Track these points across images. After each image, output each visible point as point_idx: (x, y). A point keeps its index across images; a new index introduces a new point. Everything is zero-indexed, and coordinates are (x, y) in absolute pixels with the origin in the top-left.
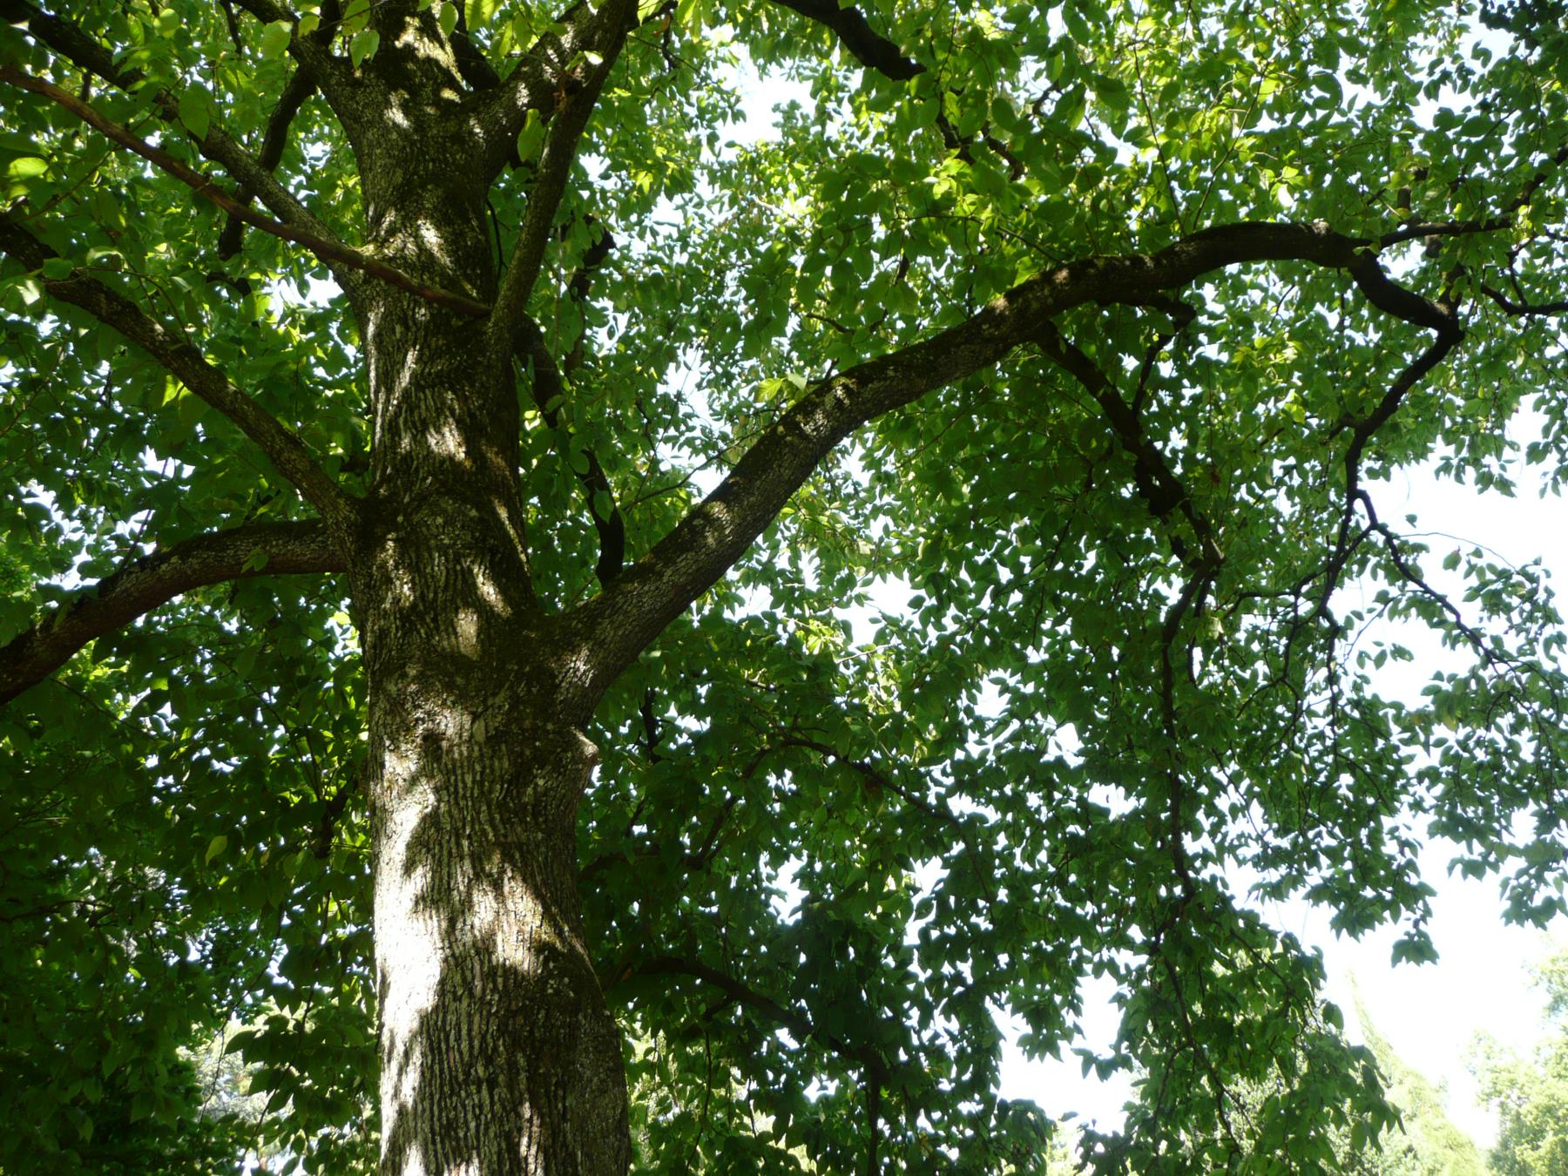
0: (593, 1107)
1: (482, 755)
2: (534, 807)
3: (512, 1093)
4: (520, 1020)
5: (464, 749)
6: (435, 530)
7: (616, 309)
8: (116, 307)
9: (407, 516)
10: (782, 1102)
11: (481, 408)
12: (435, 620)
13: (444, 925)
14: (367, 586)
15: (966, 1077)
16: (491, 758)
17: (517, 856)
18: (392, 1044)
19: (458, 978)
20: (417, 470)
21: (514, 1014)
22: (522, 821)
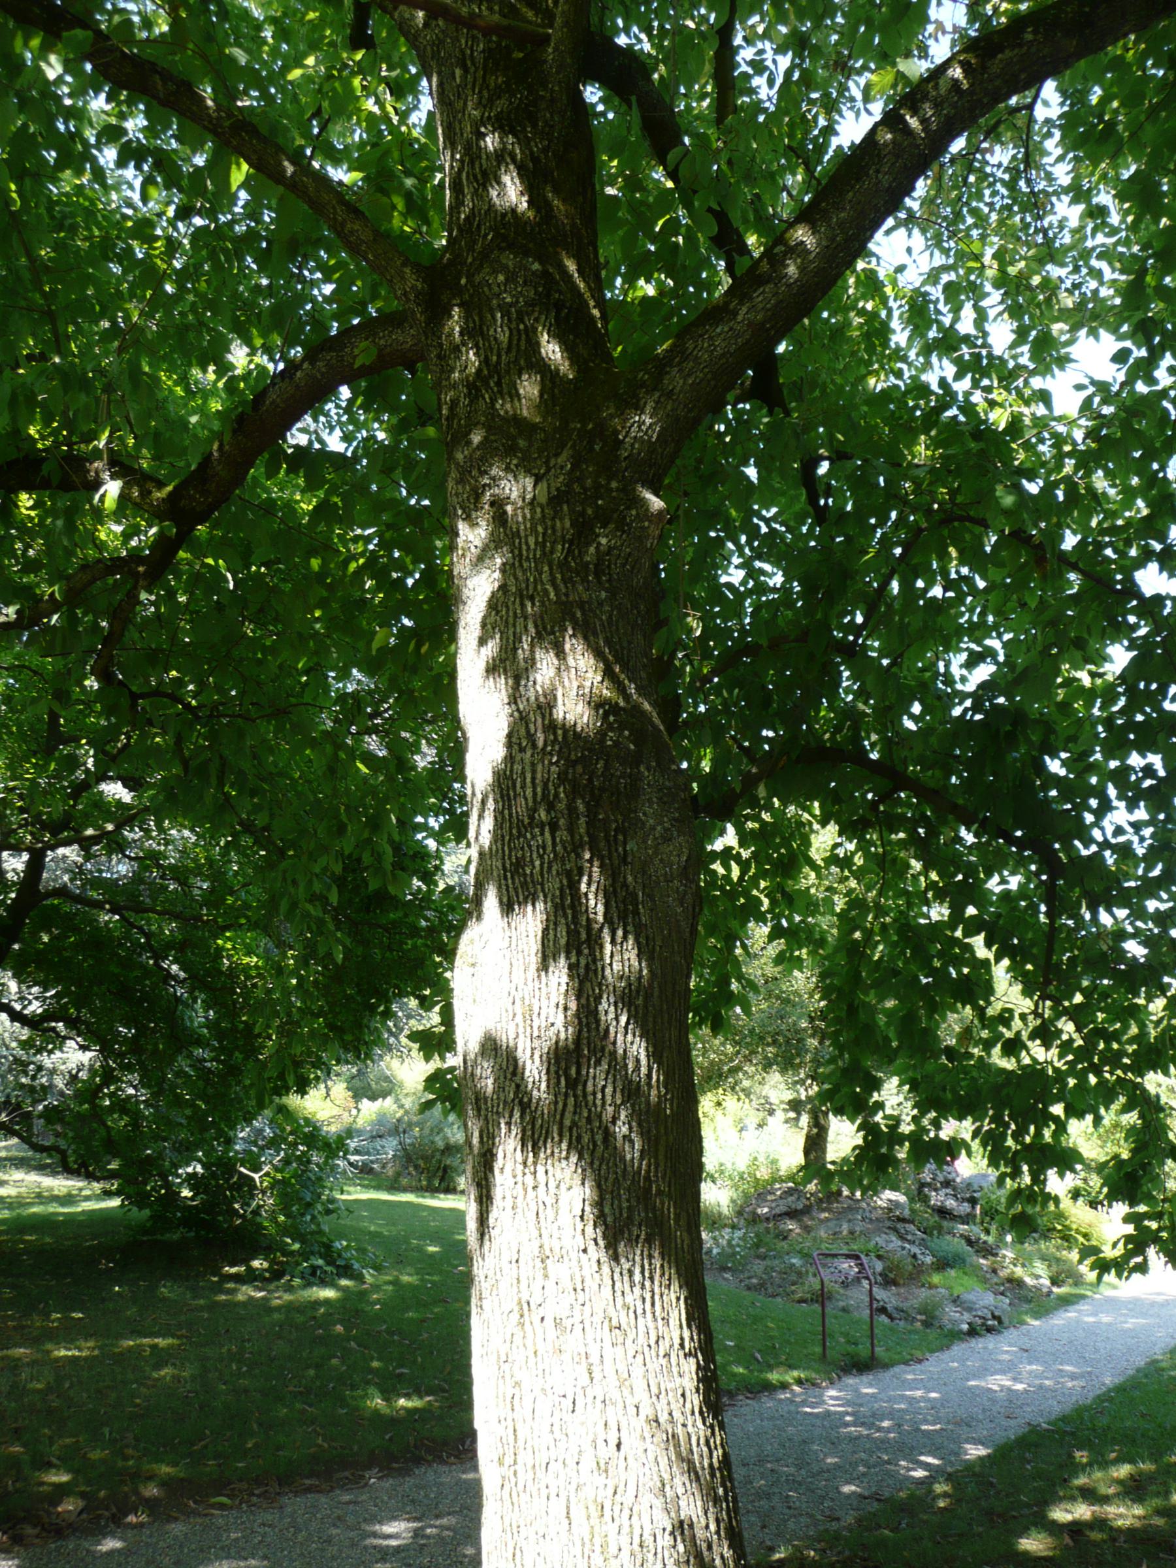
0: (656, 853)
1: (544, 516)
2: (596, 566)
3: (572, 836)
4: (579, 769)
5: (527, 511)
6: (496, 289)
7: (777, 51)
8: (172, 87)
9: (470, 277)
10: (960, 894)
11: (545, 150)
12: (499, 384)
13: (510, 682)
14: (439, 357)
15: (1156, 872)
16: (553, 519)
17: (579, 614)
18: (474, 794)
19: (523, 732)
20: (479, 226)
21: (574, 763)
22: (584, 580)
